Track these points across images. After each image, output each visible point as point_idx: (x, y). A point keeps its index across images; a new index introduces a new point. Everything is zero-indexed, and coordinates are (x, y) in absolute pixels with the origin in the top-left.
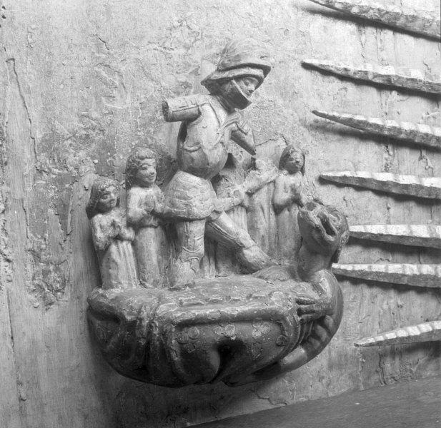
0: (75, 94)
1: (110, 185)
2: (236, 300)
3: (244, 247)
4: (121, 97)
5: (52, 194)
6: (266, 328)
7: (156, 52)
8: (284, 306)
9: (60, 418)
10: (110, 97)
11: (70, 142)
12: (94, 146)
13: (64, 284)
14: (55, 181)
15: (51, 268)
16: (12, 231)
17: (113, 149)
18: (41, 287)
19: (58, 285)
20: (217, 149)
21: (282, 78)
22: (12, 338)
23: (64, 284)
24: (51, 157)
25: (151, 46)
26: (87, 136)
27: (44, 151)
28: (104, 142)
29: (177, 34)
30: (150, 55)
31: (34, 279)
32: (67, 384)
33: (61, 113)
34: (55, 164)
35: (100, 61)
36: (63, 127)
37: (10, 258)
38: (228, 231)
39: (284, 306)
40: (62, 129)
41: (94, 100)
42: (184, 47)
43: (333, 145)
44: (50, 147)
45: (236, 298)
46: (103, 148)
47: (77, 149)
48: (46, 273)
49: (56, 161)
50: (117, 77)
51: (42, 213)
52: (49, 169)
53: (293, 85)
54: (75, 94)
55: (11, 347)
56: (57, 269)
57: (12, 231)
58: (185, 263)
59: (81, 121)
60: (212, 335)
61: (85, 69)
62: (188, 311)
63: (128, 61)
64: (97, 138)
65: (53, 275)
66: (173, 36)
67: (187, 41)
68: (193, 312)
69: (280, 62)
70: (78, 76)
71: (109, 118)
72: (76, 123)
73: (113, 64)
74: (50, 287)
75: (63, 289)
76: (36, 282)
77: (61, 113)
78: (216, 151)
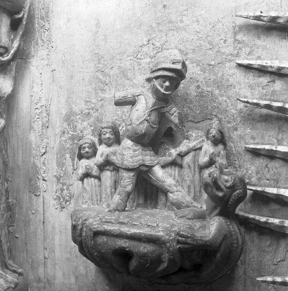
0: (84, 88)
1: (85, 143)
2: (135, 225)
3: (168, 191)
4: (110, 90)
5: (68, 146)
6: (152, 248)
7: (132, 61)
8: (167, 235)
9: (64, 274)
10: (103, 90)
11: (79, 116)
12: (92, 119)
13: (70, 198)
14: (70, 138)
15: (65, 187)
16: (48, 164)
17: (102, 122)
18: (59, 197)
19: (68, 198)
20: (143, 125)
21: (219, 75)
22: (44, 223)
23: (70, 198)
24: (69, 125)
25: (129, 58)
26: (89, 113)
27: (66, 121)
28: (98, 117)
29: (145, 49)
30: (128, 63)
31: (56, 192)
32: (69, 255)
33: (76, 100)
34: (71, 129)
35: (99, 69)
36: (76, 108)
37: (46, 179)
38: (157, 179)
39: (167, 235)
40: (76, 109)
41: (94, 91)
42: (150, 57)
43: (259, 125)
44: (69, 119)
45: (135, 223)
46: (97, 121)
47: (83, 121)
48: (62, 190)
49: (72, 127)
50: (108, 78)
51: (63, 156)
52: (68, 131)
53: (228, 80)
54: (84, 88)
55: (42, 228)
56: (68, 189)
57: (48, 164)
58: (118, 196)
59: (86, 104)
60: (114, 244)
61: (91, 74)
62: (102, 225)
63: (115, 68)
64: (94, 115)
65: (65, 192)
66: (143, 50)
67: (152, 54)
68: (104, 226)
69: (219, 64)
70: (87, 80)
71: (100, 103)
72: (83, 106)
73: (107, 71)
74: (64, 198)
75: (70, 200)
76: (57, 194)
77: (76, 100)
78: (141, 126)
